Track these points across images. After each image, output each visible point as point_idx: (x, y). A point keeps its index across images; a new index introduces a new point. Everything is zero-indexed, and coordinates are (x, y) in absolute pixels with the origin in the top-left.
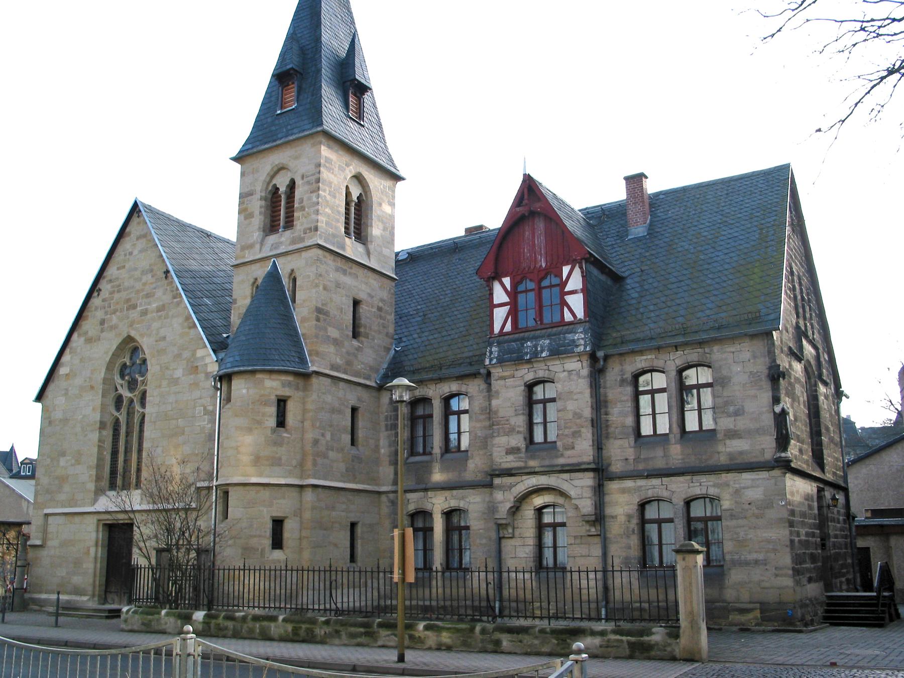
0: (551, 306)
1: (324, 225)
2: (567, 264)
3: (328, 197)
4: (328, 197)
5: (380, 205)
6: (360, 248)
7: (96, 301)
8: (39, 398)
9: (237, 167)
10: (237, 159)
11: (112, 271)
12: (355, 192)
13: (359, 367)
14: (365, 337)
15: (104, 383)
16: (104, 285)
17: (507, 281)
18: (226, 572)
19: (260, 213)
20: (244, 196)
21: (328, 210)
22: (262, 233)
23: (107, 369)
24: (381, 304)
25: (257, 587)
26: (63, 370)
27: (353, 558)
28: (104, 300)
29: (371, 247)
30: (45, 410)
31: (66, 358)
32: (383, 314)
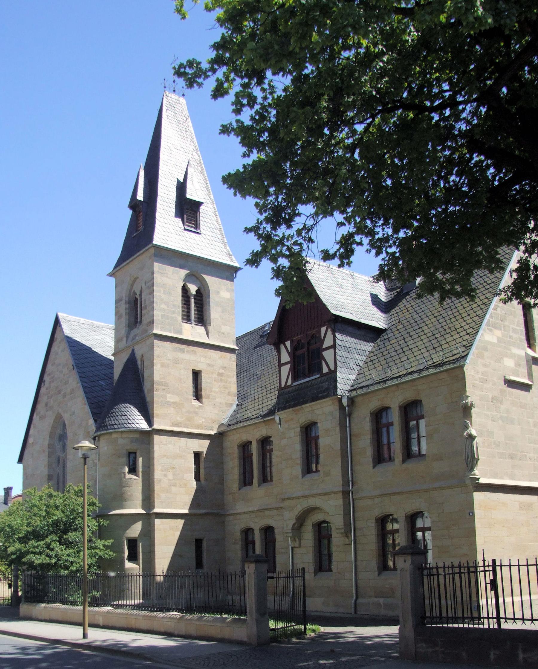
0: (447, 343)
1: (160, 318)
2: (324, 326)
3: (163, 296)
4: (163, 296)
5: (218, 293)
6: (201, 329)
7: (43, 390)
8: (20, 460)
9: (113, 280)
10: (111, 275)
11: (49, 367)
12: (193, 289)
13: (201, 421)
14: (206, 398)
15: (49, 448)
16: (46, 378)
17: (288, 344)
18: (515, 570)
19: (126, 314)
20: (117, 302)
21: (163, 306)
22: (127, 329)
23: (50, 437)
24: (221, 371)
25: (130, 584)
26: (30, 440)
27: (199, 564)
28: (47, 389)
29: (210, 328)
30: (25, 469)
31: (31, 432)
32: (223, 378)
